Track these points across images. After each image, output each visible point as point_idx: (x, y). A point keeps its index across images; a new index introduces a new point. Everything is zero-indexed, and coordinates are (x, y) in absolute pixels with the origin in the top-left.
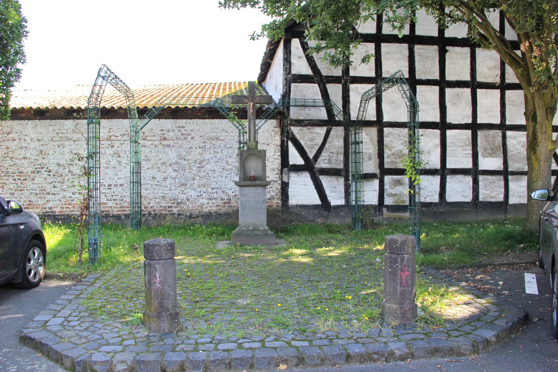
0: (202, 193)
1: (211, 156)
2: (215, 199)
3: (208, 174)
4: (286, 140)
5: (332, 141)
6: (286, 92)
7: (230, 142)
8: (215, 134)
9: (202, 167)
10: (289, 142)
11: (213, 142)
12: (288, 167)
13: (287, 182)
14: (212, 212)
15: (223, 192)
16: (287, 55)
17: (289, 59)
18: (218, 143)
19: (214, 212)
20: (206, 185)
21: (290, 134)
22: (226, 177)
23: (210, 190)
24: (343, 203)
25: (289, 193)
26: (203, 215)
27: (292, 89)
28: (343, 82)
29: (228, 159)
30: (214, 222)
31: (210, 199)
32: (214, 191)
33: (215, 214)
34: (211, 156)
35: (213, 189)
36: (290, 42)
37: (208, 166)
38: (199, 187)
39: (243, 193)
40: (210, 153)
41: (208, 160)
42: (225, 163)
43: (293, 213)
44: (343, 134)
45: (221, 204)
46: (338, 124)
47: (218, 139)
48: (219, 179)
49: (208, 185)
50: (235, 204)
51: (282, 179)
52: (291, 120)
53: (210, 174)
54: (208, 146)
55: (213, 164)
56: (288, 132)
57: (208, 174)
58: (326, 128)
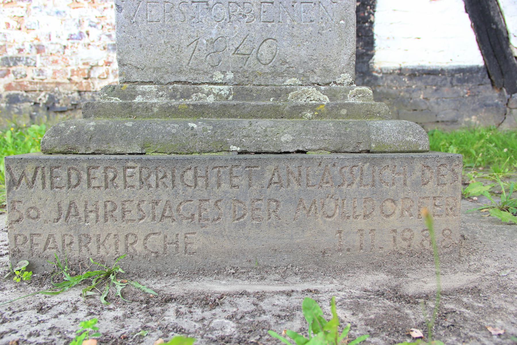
0: (86, 27)
25: (376, 30)
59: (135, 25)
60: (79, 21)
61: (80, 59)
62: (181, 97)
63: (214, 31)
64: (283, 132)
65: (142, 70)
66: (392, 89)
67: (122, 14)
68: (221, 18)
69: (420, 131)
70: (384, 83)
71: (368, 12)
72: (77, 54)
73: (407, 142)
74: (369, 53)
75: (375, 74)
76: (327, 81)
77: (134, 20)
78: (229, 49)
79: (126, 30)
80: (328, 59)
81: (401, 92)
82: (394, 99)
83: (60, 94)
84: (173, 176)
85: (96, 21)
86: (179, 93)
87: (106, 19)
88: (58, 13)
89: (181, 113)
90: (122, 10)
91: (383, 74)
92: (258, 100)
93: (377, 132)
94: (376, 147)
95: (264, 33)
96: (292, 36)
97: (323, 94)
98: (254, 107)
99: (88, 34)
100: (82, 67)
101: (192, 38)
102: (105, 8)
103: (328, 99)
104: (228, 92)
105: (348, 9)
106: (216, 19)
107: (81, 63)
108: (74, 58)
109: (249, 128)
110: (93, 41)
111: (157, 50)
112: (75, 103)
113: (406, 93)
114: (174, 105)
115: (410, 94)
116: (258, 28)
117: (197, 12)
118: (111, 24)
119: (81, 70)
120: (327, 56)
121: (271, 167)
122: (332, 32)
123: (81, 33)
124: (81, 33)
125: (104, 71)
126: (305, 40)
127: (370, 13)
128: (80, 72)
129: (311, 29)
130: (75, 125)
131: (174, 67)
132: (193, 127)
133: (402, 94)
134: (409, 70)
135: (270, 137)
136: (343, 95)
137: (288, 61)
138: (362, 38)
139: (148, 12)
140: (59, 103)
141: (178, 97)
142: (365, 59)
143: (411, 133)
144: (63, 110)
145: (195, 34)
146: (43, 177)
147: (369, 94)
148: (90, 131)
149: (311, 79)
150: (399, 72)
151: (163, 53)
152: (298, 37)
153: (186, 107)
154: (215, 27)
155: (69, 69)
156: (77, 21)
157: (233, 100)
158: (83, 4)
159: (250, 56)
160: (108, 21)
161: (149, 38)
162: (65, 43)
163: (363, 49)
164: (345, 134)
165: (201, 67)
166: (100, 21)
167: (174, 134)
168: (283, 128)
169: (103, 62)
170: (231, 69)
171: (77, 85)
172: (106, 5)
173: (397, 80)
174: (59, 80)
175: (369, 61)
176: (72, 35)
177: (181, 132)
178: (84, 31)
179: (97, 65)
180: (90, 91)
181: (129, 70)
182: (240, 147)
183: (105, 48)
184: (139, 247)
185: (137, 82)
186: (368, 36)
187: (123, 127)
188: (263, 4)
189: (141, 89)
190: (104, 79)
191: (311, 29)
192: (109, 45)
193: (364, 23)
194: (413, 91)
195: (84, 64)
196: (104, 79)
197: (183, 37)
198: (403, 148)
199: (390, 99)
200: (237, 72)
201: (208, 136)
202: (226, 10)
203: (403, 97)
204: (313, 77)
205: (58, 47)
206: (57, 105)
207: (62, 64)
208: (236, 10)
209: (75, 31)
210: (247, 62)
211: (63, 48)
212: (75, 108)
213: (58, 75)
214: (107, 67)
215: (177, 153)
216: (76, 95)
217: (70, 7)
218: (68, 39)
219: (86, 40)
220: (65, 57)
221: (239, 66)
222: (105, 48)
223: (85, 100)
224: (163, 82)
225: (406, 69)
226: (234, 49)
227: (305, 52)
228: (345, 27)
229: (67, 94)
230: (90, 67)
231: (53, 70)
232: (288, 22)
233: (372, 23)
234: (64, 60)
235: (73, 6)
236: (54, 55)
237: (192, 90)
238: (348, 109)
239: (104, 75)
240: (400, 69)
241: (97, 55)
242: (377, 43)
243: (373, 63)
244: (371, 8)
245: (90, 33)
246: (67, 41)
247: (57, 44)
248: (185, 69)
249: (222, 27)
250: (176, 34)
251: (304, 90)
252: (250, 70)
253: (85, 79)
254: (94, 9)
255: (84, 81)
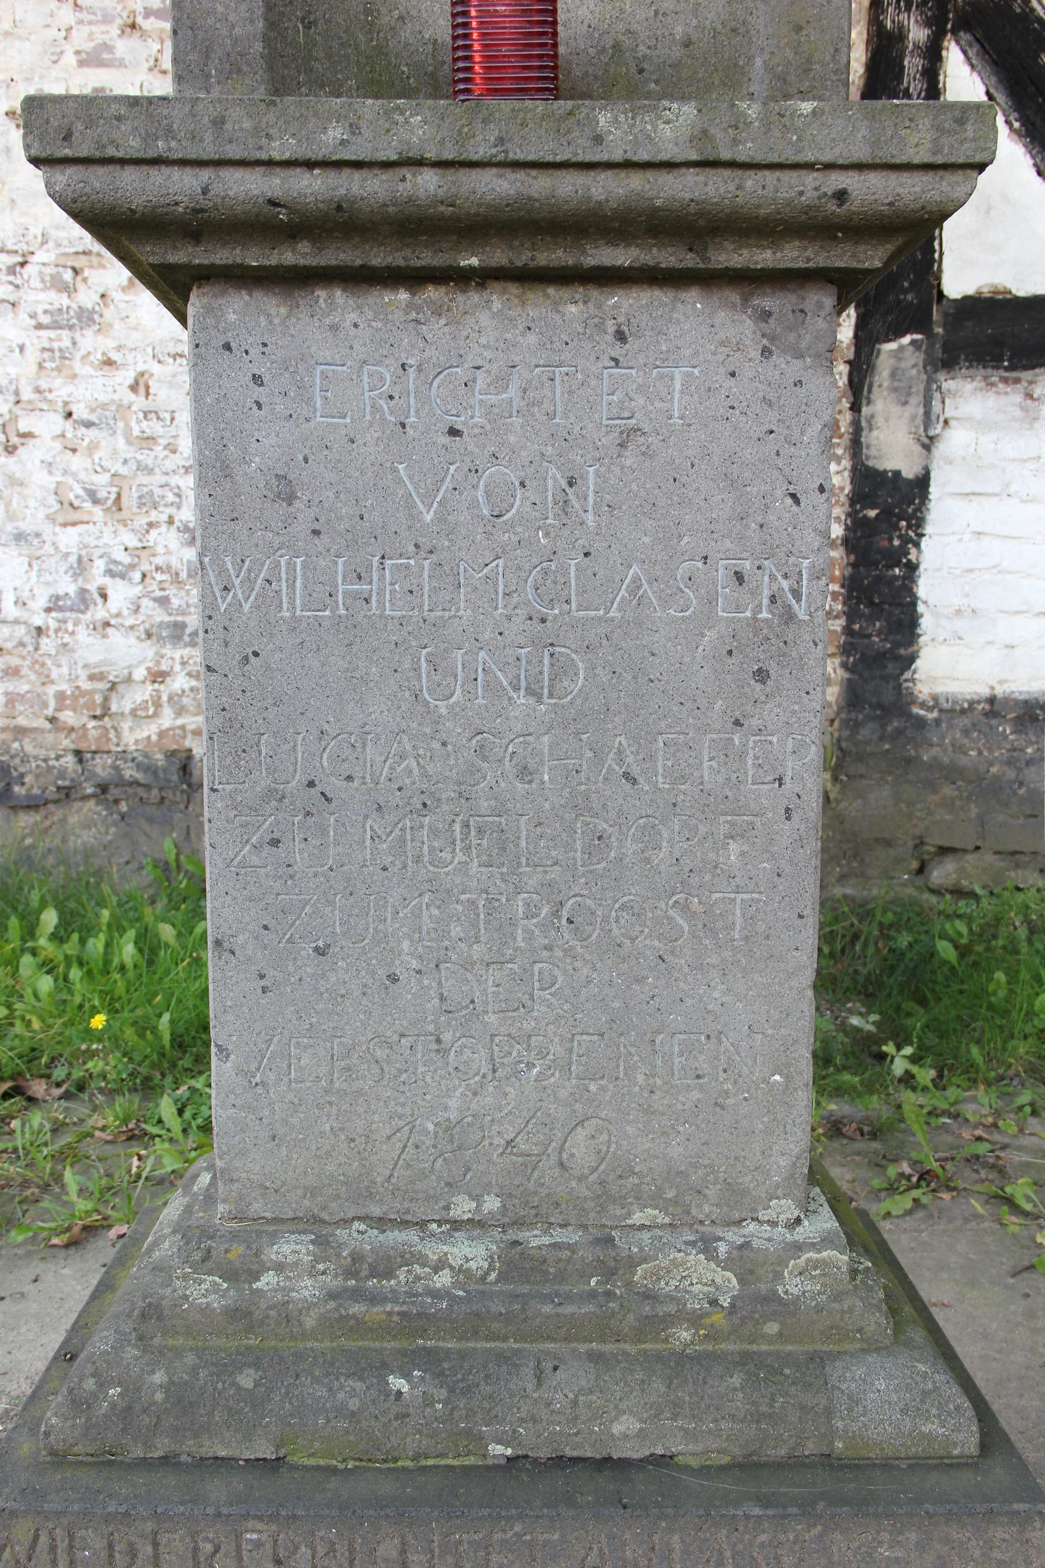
0: (97, 577)
4: (917, 34)
9: (87, 318)
12: (919, 322)
13: (909, 472)
20: (130, 500)
25: (924, 588)
38: (68, 512)
39: (266, 448)
43: (952, 773)
51: (856, 445)
59: (260, 1090)
60: (80, 560)
61: (80, 665)
62: (372, 1276)
63: (453, 1103)
64: (616, 1407)
65: (276, 1191)
66: (965, 754)
67: (228, 1064)
68: (472, 1072)
69: (957, 1408)
70: (943, 737)
71: (900, 537)
72: (73, 651)
73: (923, 1436)
74: (902, 651)
75: (916, 710)
76: (737, 1216)
77: (258, 1079)
78: (491, 1144)
79: (239, 1102)
80: (739, 1165)
81: (991, 764)
82: (971, 782)
83: (25, 759)
84: (351, 1550)
85: (125, 558)
86: (365, 1266)
87: (154, 555)
88: (20, 537)
89: (371, 1330)
90: (228, 1056)
91: (941, 711)
92: (560, 1283)
93: (850, 1410)
94: (846, 1448)
95: (577, 1106)
96: (649, 1111)
97: (723, 1269)
98: (548, 1317)
99: (104, 596)
100: (86, 685)
101: (400, 1118)
102: (151, 525)
103: (734, 1281)
104: (486, 1265)
105: (792, 1049)
106: (460, 1074)
107: (83, 675)
108: (64, 661)
109: (536, 1395)
110: (118, 615)
111: (314, 1148)
112: (67, 783)
113: (1006, 768)
114: (354, 1315)
115: (1020, 770)
116: (563, 1094)
117: (413, 1059)
118: (169, 567)
119: (83, 693)
120: (736, 1158)
122: (751, 1102)
123: (83, 592)
124: (83, 592)
125: (147, 697)
126: (682, 1120)
127: (906, 540)
128: (82, 701)
129: (696, 1095)
130: (120, 1384)
131: (354, 1186)
132: (399, 1393)
133: (994, 770)
134: (1016, 702)
135: (584, 1423)
136: (774, 1272)
137: (637, 1170)
138: (882, 610)
139: (294, 1061)
140: (23, 784)
141: (364, 1274)
142: (891, 668)
143: (934, 1411)
144: (33, 803)
145: (407, 1110)
146: (53, 1548)
147: (839, 1268)
148: (155, 1403)
149: (694, 1211)
150: (987, 707)
151: (328, 1155)
152: (663, 1114)
153: (384, 1317)
154: (458, 1094)
155: (51, 690)
156: (73, 559)
157: (497, 1281)
158: (90, 513)
159: (544, 1157)
160: (159, 561)
161: (294, 1121)
162: (38, 621)
163: (886, 640)
164: (770, 1416)
165: (419, 1186)
166: (136, 560)
167: (353, 1414)
168: (618, 1395)
169: (145, 673)
170: (496, 1190)
171: (74, 735)
172: (154, 516)
173: (980, 732)
174: (22, 721)
175: (902, 674)
176: (58, 598)
177: (371, 1408)
178: (92, 587)
180: (109, 752)
181: (244, 1191)
182: (513, 1448)
183: (149, 635)
185: (263, 1218)
186: (900, 605)
187: (231, 1392)
188: (578, 1037)
189: (273, 1257)
190: (148, 717)
191: (696, 1095)
192: (161, 625)
193: (891, 567)
194: (1028, 763)
195: (91, 678)
196: (148, 717)
197: (376, 1118)
198: (913, 1450)
199: (959, 783)
200: (511, 1195)
201: (436, 1419)
202: (483, 1053)
203: (996, 778)
204: (699, 1206)
205: (21, 631)
206: (17, 789)
207: (33, 677)
208: (510, 1053)
209: (68, 587)
210: (536, 1174)
211: (34, 632)
212: (67, 796)
213: (20, 707)
214: (156, 686)
215: (361, 1460)
216: (69, 760)
217: (54, 521)
218: (48, 610)
219: (99, 613)
220: (41, 659)
221: (516, 1182)
222: (149, 635)
223: (94, 775)
224: (327, 1218)
225: (1009, 702)
226: (503, 1142)
227: (681, 1149)
228: (784, 1092)
229: (45, 760)
230: (109, 685)
231: (7, 694)
232: (640, 1078)
233: (912, 568)
234: (37, 667)
235: (61, 519)
236: (10, 653)
237: (399, 1260)
238: (782, 1324)
239: (147, 709)
240: (992, 700)
241: (127, 652)
242: (926, 623)
243: (913, 680)
244: (909, 527)
245: (109, 592)
246: (43, 615)
247: (17, 622)
248: (381, 1190)
249: (475, 1094)
250: (360, 1109)
251: (675, 1259)
252: (544, 1192)
253: (95, 717)
254: (120, 527)
255: (92, 724)
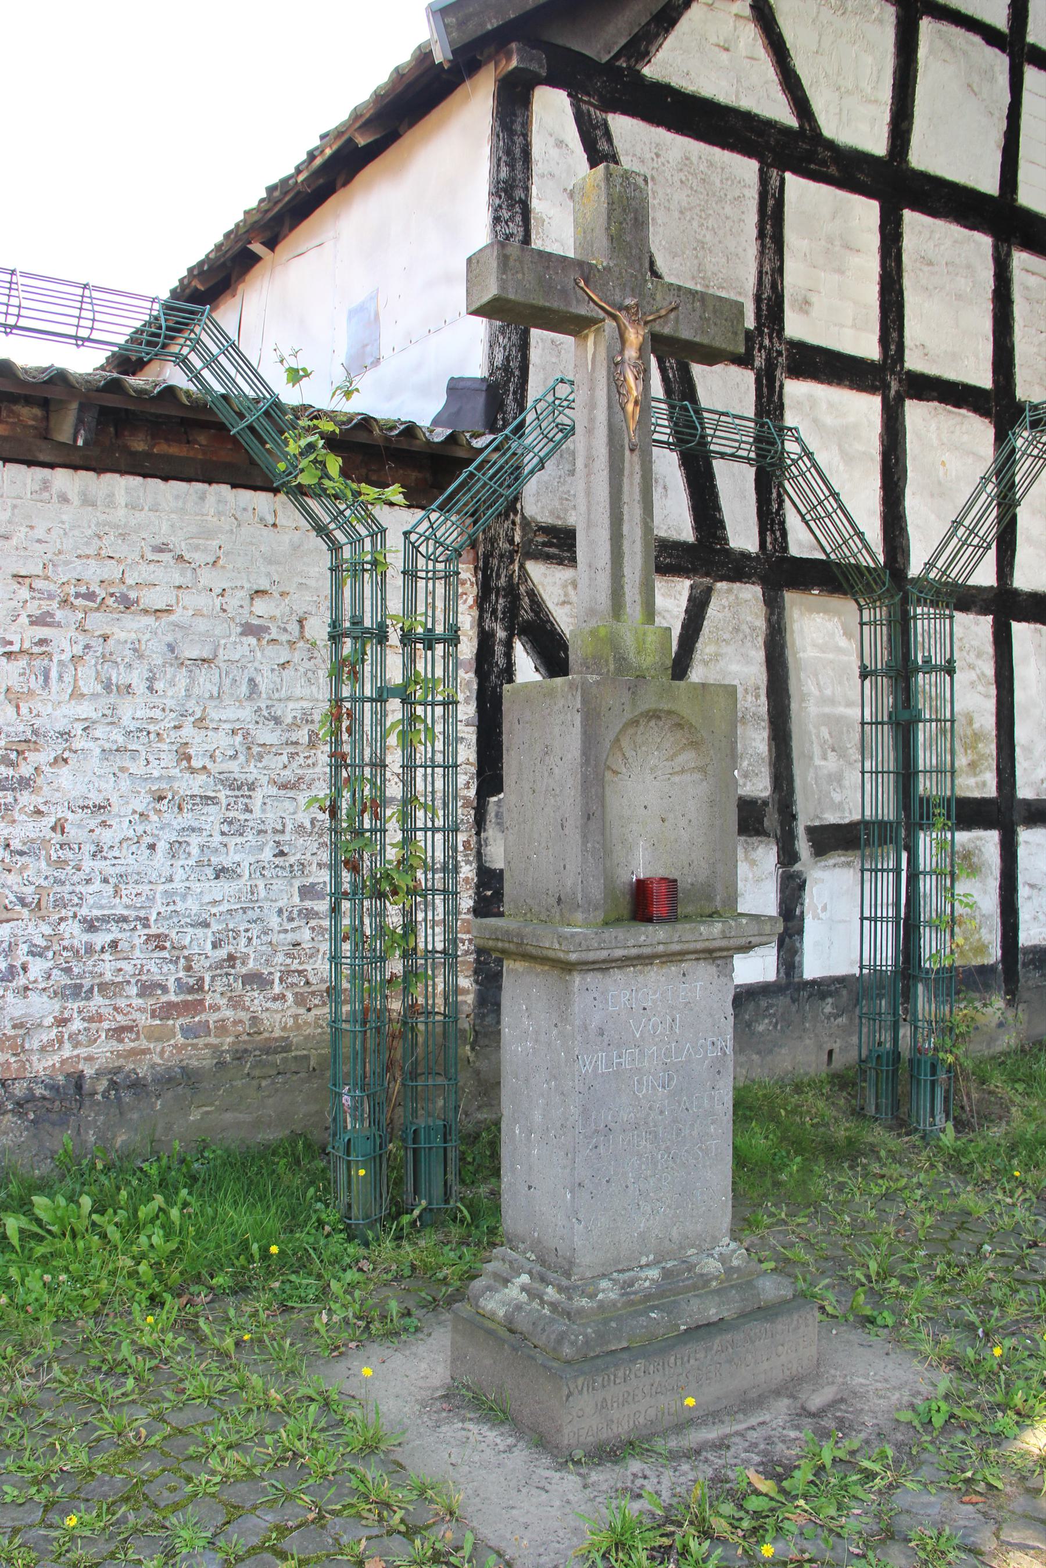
1: (85, 710)
2: (103, 987)
3: (59, 827)
4: (501, 634)
5: (717, 657)
6: (506, 368)
7: (202, 625)
8: (112, 571)
9: (25, 783)
10: (519, 649)
11: (97, 622)
14: (89, 1071)
15: (158, 942)
16: (511, 166)
17: (519, 194)
18: (128, 629)
19: (99, 1074)
20: (48, 902)
21: (526, 602)
22: (175, 849)
23: (73, 932)
24: (771, 976)
26: (31, 1098)
27: (535, 355)
28: (759, 361)
29: (188, 731)
30: (101, 1137)
31: (76, 992)
32: (101, 939)
33: (103, 1085)
34: (85, 710)
35: (91, 926)
36: (526, 103)
37: (64, 776)
40: (76, 695)
41: (65, 735)
42: (169, 759)
44: (761, 624)
45: (144, 1020)
46: (739, 568)
47: (127, 604)
48: (131, 860)
49: (61, 903)
50: (229, 1013)
51: (479, 855)
52: (526, 523)
53: (73, 833)
54: (64, 642)
55: (94, 762)
56: (512, 592)
57: (59, 827)
58: (688, 583)
110: (35, 982)
121: (717, 1341)
123: (12, 967)
124: (12, 967)
178: (18, 964)
179: (40, 1025)
184: (641, 1420)
195: (14, 1027)
219: (21, 981)
